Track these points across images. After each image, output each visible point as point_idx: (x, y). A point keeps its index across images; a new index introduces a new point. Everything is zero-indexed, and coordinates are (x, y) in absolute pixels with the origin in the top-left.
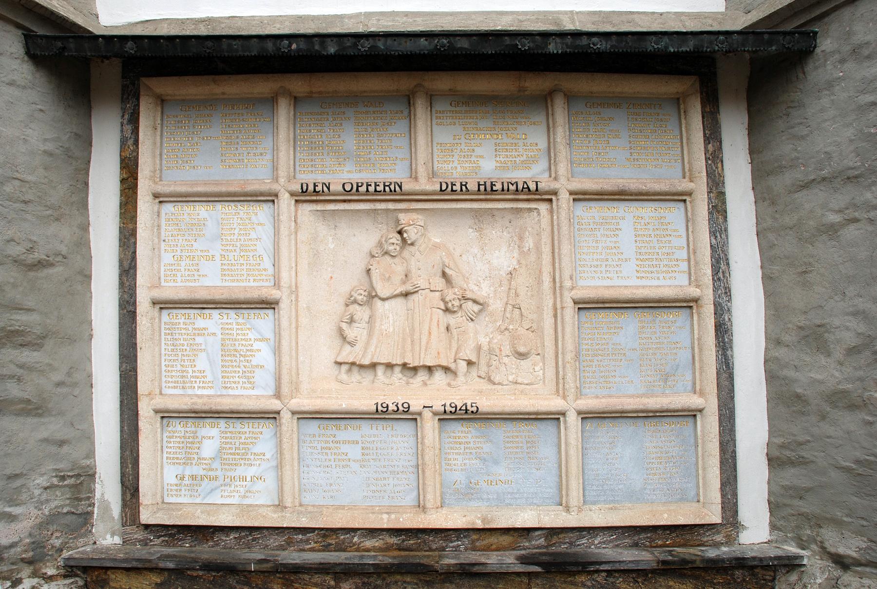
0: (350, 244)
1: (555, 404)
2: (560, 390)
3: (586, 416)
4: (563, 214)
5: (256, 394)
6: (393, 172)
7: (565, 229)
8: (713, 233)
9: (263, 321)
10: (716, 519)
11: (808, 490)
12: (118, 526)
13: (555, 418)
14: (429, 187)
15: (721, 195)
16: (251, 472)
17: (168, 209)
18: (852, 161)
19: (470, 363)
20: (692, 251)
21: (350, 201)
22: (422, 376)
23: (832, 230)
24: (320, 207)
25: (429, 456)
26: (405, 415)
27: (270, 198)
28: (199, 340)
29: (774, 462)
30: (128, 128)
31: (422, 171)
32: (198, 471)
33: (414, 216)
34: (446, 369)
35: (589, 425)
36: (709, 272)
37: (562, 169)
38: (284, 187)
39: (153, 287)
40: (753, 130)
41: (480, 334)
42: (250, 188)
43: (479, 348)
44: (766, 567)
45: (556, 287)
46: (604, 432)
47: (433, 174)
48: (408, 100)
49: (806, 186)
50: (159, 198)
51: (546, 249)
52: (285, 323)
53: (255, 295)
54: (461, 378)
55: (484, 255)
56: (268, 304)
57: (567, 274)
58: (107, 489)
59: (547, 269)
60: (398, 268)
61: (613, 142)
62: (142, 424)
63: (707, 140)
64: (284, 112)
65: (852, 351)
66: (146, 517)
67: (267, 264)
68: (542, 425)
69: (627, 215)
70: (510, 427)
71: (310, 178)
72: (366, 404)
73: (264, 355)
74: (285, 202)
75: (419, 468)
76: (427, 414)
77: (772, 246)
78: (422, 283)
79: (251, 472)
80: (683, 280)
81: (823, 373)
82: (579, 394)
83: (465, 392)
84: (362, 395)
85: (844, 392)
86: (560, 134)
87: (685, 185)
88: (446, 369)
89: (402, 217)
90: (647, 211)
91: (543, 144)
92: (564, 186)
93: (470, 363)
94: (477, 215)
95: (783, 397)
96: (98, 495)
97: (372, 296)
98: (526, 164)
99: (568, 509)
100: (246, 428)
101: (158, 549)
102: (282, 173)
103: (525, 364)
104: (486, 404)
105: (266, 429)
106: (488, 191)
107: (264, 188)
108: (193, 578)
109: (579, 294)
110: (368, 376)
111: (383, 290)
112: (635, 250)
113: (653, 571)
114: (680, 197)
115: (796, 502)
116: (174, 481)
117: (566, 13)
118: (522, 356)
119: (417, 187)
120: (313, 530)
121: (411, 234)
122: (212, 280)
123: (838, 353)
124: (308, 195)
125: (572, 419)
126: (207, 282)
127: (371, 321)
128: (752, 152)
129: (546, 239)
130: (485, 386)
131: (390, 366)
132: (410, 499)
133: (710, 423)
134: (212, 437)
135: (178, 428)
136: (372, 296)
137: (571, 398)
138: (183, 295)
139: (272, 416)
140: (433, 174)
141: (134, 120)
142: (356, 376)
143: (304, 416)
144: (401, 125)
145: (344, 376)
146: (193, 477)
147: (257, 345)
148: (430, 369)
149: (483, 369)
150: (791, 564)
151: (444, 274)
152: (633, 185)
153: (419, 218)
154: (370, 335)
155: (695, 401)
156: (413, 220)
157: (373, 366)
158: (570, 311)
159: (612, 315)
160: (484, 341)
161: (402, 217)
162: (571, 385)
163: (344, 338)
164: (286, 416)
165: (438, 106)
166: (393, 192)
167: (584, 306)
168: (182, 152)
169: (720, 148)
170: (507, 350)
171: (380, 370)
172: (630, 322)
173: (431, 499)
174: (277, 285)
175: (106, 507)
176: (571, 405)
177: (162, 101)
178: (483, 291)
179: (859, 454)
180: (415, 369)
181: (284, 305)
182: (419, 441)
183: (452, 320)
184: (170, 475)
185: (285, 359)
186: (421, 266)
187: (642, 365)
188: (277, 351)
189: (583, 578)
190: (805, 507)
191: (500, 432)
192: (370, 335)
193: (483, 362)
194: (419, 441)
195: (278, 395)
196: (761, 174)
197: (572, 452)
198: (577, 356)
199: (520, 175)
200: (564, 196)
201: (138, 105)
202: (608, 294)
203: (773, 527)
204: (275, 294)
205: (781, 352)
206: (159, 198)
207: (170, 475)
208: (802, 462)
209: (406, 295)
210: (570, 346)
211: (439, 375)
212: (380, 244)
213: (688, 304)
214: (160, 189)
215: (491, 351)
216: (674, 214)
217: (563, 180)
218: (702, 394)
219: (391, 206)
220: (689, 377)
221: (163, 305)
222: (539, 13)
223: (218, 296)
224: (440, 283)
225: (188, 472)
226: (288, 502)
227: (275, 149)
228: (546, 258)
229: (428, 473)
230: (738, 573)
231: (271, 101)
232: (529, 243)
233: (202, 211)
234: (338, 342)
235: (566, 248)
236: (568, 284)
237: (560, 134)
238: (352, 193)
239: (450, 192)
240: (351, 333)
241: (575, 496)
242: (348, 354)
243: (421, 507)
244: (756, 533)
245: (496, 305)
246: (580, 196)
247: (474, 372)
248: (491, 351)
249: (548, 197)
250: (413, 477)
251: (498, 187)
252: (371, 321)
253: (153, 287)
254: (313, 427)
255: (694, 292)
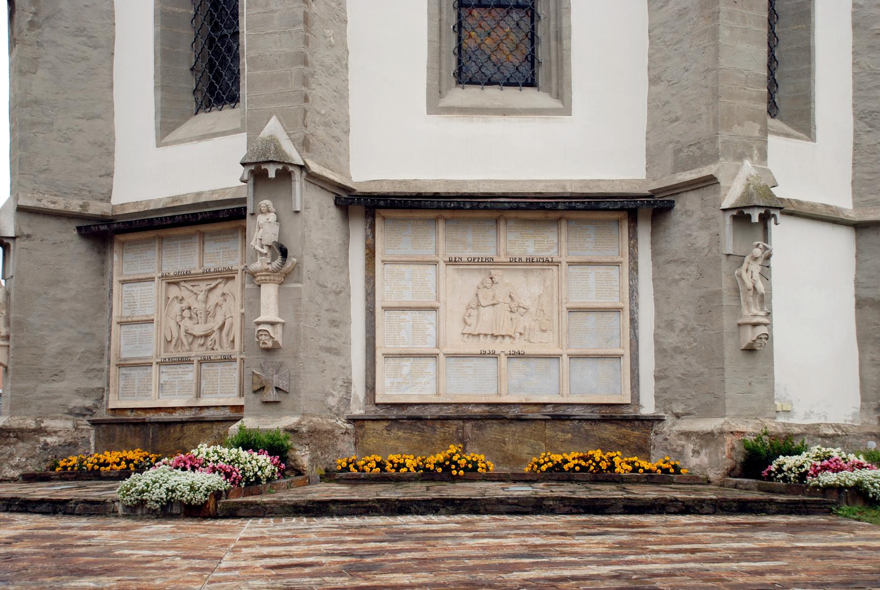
0: (469, 282)
1: (557, 351)
2: (560, 345)
3: (572, 357)
4: (563, 272)
5: (428, 347)
6: (489, 252)
7: (564, 278)
8: (630, 279)
9: (431, 316)
10: (628, 401)
11: (667, 389)
12: (362, 405)
13: (557, 357)
14: (505, 260)
15: (636, 263)
16: (424, 380)
17: (388, 266)
18: (683, 256)
19: (521, 334)
20: (621, 287)
21: (424, 532)
22: (500, 339)
23: (676, 282)
24: (456, 267)
25: (503, 372)
26: (493, 355)
27: (436, 263)
28: (402, 324)
29: (657, 378)
30: (369, 231)
31: (502, 253)
32: (400, 380)
33: (498, 271)
34: (510, 336)
35: (572, 361)
36: (628, 296)
37: (564, 252)
38: (442, 258)
39: (383, 301)
40: (653, 234)
41: (525, 322)
42: (426, 259)
43: (525, 328)
44: (648, 420)
45: (559, 302)
46: (580, 363)
47: (507, 254)
48: (497, 221)
49: (669, 262)
50: (384, 262)
51: (556, 286)
52: (441, 316)
53: (429, 305)
54: (517, 340)
55: (528, 288)
56: (434, 309)
57: (564, 296)
58: (358, 389)
59: (555, 294)
60: (490, 293)
61: (587, 240)
62: (377, 360)
63: (630, 238)
64: (441, 225)
65: (682, 330)
66: (378, 400)
67: (433, 291)
68: (552, 360)
69: (592, 272)
70: (539, 361)
71: (453, 255)
72: (477, 351)
73: (431, 330)
74: (442, 265)
75: (498, 378)
76: (503, 355)
77: (657, 286)
78: (500, 300)
79: (424, 380)
80: (617, 300)
81: (672, 339)
82: (568, 347)
83: (519, 346)
84: (474, 347)
85: (678, 347)
86: (563, 237)
87: (619, 259)
88: (510, 336)
89: (492, 271)
90: (602, 270)
91: (555, 241)
92: (564, 260)
93: (521, 334)
94: (525, 271)
95: (660, 351)
96: (353, 392)
97: (479, 305)
98: (548, 249)
99: (562, 396)
100: (423, 361)
101: (381, 412)
102: (441, 253)
103: (545, 334)
104: (527, 351)
105: (431, 362)
106: (531, 261)
107: (432, 259)
108: (402, 423)
109: (569, 305)
110: (476, 339)
111: (483, 303)
112: (600, 286)
113: (599, 420)
114: (617, 264)
115: (664, 394)
116: (389, 385)
117: (568, 181)
118: (544, 331)
119: (500, 260)
120: (451, 404)
121: (496, 279)
122: (408, 298)
123: (677, 331)
124: (452, 262)
125: (565, 357)
126: (405, 299)
127: (478, 316)
128: (652, 244)
129: (555, 281)
130: (527, 343)
131: (486, 335)
132: (494, 391)
133: (626, 361)
134: (407, 365)
135: (391, 361)
136: (479, 305)
137: (564, 348)
138: (397, 305)
139: (435, 356)
140: (507, 254)
141: (373, 227)
142: (471, 339)
143: (449, 356)
144: (493, 232)
145: (466, 339)
146: (398, 383)
147: (428, 326)
148: (503, 336)
149: (527, 337)
150: (660, 420)
151: (510, 296)
152: (595, 260)
153: (500, 272)
154: (477, 322)
155: (620, 351)
156: (497, 273)
157: (479, 335)
158: (565, 313)
159: (584, 314)
160: (527, 325)
161: (492, 271)
162: (565, 343)
163: (466, 323)
164: (441, 356)
165: (510, 224)
166: (489, 261)
167: (571, 310)
168: (395, 241)
169: (637, 242)
170: (537, 328)
171: (482, 337)
172: (592, 317)
173: (504, 390)
174: (438, 300)
175: (357, 398)
176: (564, 352)
177: (384, 218)
178: (527, 303)
179: (682, 371)
180: (497, 336)
181: (440, 309)
182: (498, 366)
183: (513, 316)
184: (388, 382)
185: (442, 332)
186: (501, 293)
187: (610, 335)
188: (438, 328)
189: (568, 422)
190: (666, 396)
191: (533, 362)
192: (477, 322)
193: (527, 333)
194: (498, 366)
195: (438, 347)
196: (655, 254)
197: (565, 371)
198: (568, 331)
199: (545, 255)
200: (564, 264)
201: (374, 221)
202: (582, 306)
203: (656, 407)
204: (437, 304)
205: (660, 331)
206: (384, 262)
207: (388, 382)
208: (666, 377)
209: (494, 305)
210: (565, 327)
211: (507, 339)
212: (482, 283)
213: (618, 310)
214: (385, 259)
215: (530, 329)
216: (614, 271)
217: (564, 257)
218: (623, 348)
219: (488, 267)
220: (618, 341)
221: (386, 309)
222: (556, 181)
223: (412, 305)
224: (508, 300)
225: (396, 381)
226: (441, 392)
227: (437, 242)
228: (555, 290)
229: (502, 379)
230: (636, 423)
231: (436, 220)
232: (548, 283)
233: (403, 268)
234: (463, 324)
235: (564, 286)
236: (564, 301)
237: (563, 237)
238: (472, 261)
239: (514, 262)
240: (469, 321)
241: (566, 391)
242: (468, 330)
243: (499, 394)
244: (648, 408)
245: (533, 309)
246: (571, 264)
247: (522, 337)
248: (530, 329)
249: (557, 264)
250: (495, 382)
251: (535, 260)
252: (478, 316)
253: (383, 301)
254: (452, 361)
255: (621, 305)
